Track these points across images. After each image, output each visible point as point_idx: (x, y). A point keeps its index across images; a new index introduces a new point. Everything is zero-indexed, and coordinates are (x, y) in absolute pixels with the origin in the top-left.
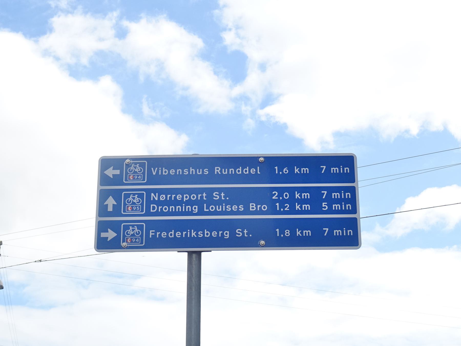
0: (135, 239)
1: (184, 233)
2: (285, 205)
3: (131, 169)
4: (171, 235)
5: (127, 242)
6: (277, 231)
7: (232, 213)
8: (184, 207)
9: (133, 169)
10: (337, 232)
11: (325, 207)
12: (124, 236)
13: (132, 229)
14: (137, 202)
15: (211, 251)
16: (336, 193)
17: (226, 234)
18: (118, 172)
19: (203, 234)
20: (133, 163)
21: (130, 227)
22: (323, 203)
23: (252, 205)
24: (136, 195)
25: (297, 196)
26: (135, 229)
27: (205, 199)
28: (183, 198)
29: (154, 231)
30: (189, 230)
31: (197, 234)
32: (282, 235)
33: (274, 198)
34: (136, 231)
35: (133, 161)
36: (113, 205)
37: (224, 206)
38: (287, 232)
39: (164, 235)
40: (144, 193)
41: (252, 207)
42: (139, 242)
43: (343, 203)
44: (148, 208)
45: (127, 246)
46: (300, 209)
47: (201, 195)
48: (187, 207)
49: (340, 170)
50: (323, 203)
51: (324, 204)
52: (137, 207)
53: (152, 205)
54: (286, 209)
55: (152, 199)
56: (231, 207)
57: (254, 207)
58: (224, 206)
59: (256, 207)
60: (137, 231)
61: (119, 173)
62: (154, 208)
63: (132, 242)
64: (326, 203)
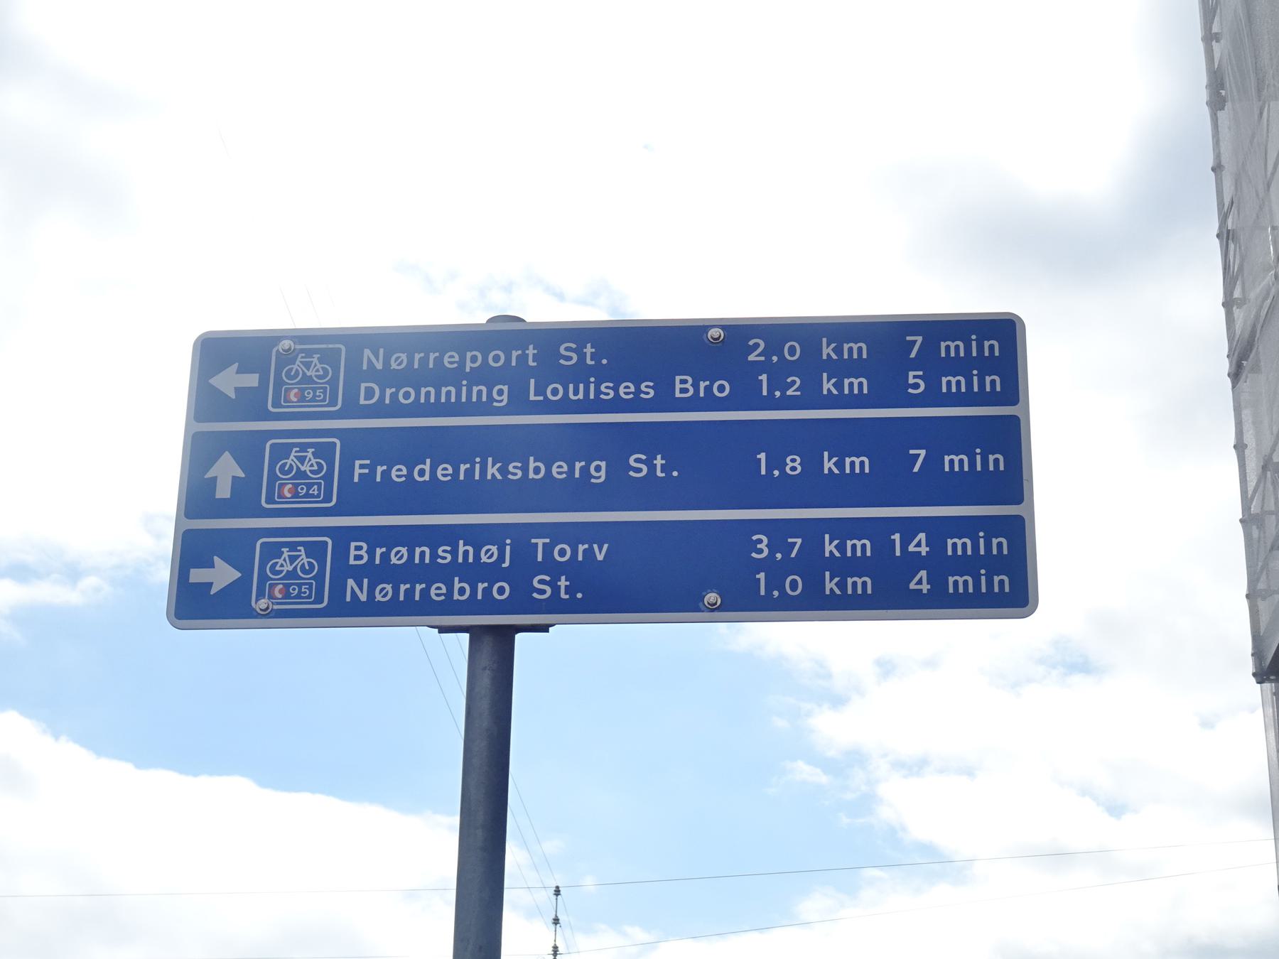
0: (305, 488)
1: (463, 467)
2: (789, 380)
3: (292, 368)
4: (422, 473)
5: (271, 597)
6: (759, 579)
7: (617, 405)
8: (464, 389)
9: (300, 370)
10: (954, 461)
11: (916, 386)
12: (263, 578)
13: (289, 556)
14: (316, 376)
15: (544, 628)
16: (953, 342)
17: (598, 469)
18: (252, 380)
19: (525, 469)
20: (302, 351)
21: (282, 549)
22: (911, 374)
23: (681, 380)
24: (311, 450)
25: (830, 548)
26: (300, 555)
27: (531, 363)
28: (462, 363)
29: (368, 462)
30: (478, 460)
31: (503, 471)
32: (776, 473)
33: (751, 358)
34: (302, 562)
35: (301, 344)
36: (234, 478)
37: (592, 386)
38: (793, 461)
39: (398, 473)
40: (340, 349)
41: (683, 385)
42: (318, 496)
43: (978, 451)
44: (338, 588)
45: (272, 609)
46: (838, 472)
47: (520, 352)
48: (475, 389)
49: (976, 547)
50: (911, 374)
51: (915, 377)
52: (304, 587)
53: (363, 386)
54: (789, 393)
55: (348, 599)
56: (616, 389)
57: (688, 386)
58: (592, 386)
59: (696, 386)
60: (304, 563)
61: (256, 384)
62: (370, 392)
63: (287, 595)
64: (920, 373)
